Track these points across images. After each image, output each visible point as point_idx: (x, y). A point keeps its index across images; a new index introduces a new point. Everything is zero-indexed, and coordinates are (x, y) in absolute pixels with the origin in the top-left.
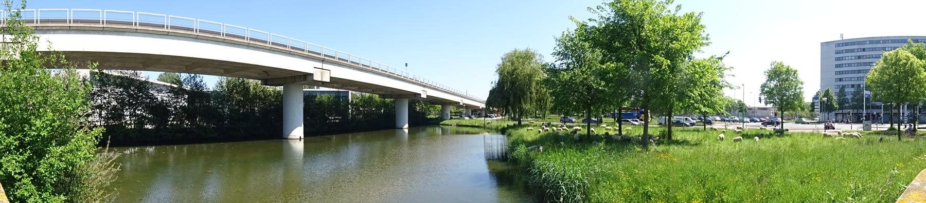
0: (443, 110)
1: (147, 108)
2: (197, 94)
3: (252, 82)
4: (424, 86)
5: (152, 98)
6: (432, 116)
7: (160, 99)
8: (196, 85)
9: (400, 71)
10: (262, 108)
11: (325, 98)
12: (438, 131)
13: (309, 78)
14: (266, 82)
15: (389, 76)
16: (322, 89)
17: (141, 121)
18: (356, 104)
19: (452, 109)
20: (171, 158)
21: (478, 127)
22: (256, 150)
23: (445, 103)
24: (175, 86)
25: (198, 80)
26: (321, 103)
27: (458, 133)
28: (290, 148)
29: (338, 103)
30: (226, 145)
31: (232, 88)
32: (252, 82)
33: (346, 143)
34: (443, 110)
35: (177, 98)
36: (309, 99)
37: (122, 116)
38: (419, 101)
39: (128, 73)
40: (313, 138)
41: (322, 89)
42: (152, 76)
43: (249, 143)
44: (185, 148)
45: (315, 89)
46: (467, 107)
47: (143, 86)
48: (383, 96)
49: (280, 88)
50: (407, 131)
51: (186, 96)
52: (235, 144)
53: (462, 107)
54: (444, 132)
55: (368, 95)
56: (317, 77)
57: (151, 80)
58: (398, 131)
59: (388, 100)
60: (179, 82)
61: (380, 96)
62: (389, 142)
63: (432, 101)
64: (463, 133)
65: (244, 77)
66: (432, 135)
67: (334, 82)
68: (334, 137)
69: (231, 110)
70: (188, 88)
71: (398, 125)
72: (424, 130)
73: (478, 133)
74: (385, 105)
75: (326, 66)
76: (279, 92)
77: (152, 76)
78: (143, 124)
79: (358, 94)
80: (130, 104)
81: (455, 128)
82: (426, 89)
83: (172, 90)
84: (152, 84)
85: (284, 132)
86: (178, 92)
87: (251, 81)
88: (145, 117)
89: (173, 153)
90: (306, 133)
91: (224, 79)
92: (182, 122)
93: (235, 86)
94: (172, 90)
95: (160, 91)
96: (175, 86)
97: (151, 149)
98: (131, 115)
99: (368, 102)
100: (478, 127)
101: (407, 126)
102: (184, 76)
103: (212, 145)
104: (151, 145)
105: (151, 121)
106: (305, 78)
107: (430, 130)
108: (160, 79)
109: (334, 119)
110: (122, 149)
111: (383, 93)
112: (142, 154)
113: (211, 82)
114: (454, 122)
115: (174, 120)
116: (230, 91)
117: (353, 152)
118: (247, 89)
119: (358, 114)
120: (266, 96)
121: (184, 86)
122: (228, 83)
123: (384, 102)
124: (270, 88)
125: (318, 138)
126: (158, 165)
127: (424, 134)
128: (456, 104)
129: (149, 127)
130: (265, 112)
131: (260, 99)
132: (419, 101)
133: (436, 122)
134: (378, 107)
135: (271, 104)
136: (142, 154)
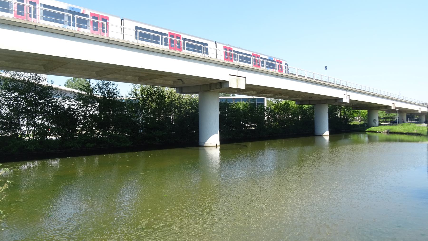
0: (369, 116)
1: (48, 116)
2: (110, 102)
3: (167, 90)
4: (347, 90)
5: (57, 107)
6: (356, 123)
7: (66, 106)
8: (109, 92)
9: (318, 74)
10: (178, 117)
11: (240, 105)
12: (364, 138)
13: (225, 86)
14: (181, 90)
15: (307, 81)
16: (237, 96)
17: (42, 131)
18: (272, 111)
19: (381, 114)
20: (80, 170)
21: (417, 134)
22: (172, 158)
23: (371, 108)
24: (84, 93)
25: (111, 87)
26: (238, 109)
27: (388, 140)
28: (205, 154)
29: (254, 111)
30: (142, 154)
31: (147, 97)
32: (167, 90)
33: (263, 148)
34: (369, 116)
35: (87, 106)
36: (224, 106)
37: (19, 126)
38: (340, 107)
39: (26, 76)
40: (229, 146)
41: (237, 96)
42: (58, 82)
43: (166, 151)
44: (96, 159)
45: (231, 97)
46: (401, 111)
47: (46, 92)
48: (301, 102)
49: (196, 96)
50: (327, 138)
51: (98, 104)
52: (152, 153)
53: (394, 111)
54: (371, 139)
55: (283, 101)
56: (233, 85)
57: (54, 86)
58: (317, 139)
59: (305, 106)
60: (88, 89)
61: (298, 102)
62: (308, 149)
63: (357, 106)
64: (396, 141)
65: (159, 85)
66: (358, 142)
67: (249, 89)
68: (250, 144)
69: (146, 119)
70: (99, 95)
71: (318, 132)
72: (346, 138)
73: (417, 141)
74: (303, 112)
75: (241, 73)
76: (195, 101)
77: (58, 82)
78: (45, 134)
79: (273, 101)
80: (28, 113)
81: (384, 136)
82: (348, 93)
83: (80, 97)
84: (57, 89)
85: (201, 140)
86: (87, 99)
87: (166, 89)
88: (48, 127)
89: (81, 165)
90: (222, 141)
91: (138, 87)
92: (93, 132)
93: (149, 94)
94: (80, 97)
95: (68, 98)
96: (84, 93)
97: (55, 163)
98: (28, 124)
99: (286, 108)
100: (417, 134)
101: (327, 133)
102: (94, 83)
103: (126, 155)
104: (54, 157)
105: (54, 131)
106: (220, 85)
107: (354, 137)
108: (68, 84)
109: (250, 126)
110: (16, 164)
111: (300, 99)
112: (43, 168)
113: (125, 90)
114: (384, 128)
115: (83, 129)
116: (145, 100)
117: (270, 157)
118: (161, 97)
119: (274, 122)
120: (181, 106)
121: (95, 94)
122: (143, 90)
123: (302, 109)
124: (186, 96)
125: (234, 145)
126: (64, 179)
127: (346, 141)
128: (387, 108)
129: (53, 138)
130: (181, 120)
131: (176, 107)
132: (340, 107)
133: (361, 129)
134: (295, 113)
135: (187, 111)
136: (43, 168)
